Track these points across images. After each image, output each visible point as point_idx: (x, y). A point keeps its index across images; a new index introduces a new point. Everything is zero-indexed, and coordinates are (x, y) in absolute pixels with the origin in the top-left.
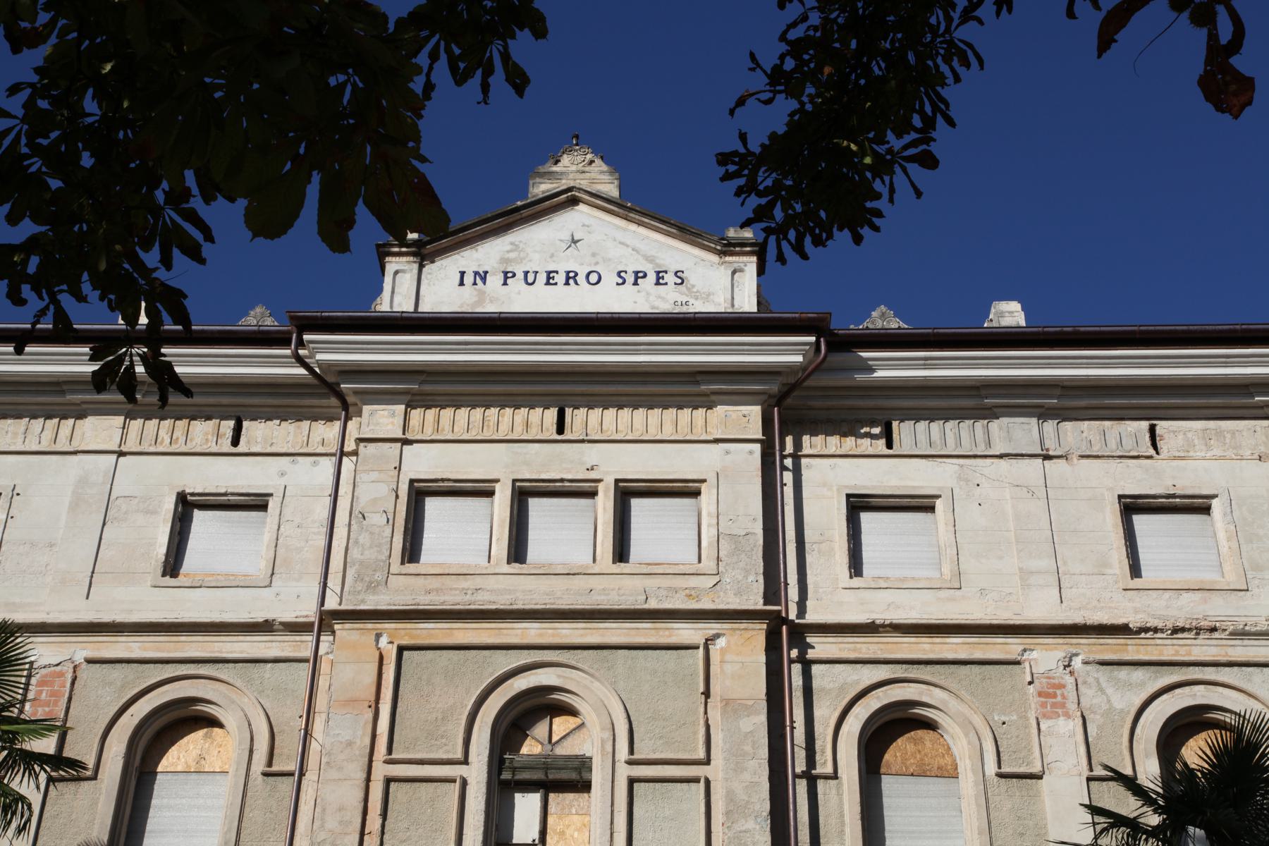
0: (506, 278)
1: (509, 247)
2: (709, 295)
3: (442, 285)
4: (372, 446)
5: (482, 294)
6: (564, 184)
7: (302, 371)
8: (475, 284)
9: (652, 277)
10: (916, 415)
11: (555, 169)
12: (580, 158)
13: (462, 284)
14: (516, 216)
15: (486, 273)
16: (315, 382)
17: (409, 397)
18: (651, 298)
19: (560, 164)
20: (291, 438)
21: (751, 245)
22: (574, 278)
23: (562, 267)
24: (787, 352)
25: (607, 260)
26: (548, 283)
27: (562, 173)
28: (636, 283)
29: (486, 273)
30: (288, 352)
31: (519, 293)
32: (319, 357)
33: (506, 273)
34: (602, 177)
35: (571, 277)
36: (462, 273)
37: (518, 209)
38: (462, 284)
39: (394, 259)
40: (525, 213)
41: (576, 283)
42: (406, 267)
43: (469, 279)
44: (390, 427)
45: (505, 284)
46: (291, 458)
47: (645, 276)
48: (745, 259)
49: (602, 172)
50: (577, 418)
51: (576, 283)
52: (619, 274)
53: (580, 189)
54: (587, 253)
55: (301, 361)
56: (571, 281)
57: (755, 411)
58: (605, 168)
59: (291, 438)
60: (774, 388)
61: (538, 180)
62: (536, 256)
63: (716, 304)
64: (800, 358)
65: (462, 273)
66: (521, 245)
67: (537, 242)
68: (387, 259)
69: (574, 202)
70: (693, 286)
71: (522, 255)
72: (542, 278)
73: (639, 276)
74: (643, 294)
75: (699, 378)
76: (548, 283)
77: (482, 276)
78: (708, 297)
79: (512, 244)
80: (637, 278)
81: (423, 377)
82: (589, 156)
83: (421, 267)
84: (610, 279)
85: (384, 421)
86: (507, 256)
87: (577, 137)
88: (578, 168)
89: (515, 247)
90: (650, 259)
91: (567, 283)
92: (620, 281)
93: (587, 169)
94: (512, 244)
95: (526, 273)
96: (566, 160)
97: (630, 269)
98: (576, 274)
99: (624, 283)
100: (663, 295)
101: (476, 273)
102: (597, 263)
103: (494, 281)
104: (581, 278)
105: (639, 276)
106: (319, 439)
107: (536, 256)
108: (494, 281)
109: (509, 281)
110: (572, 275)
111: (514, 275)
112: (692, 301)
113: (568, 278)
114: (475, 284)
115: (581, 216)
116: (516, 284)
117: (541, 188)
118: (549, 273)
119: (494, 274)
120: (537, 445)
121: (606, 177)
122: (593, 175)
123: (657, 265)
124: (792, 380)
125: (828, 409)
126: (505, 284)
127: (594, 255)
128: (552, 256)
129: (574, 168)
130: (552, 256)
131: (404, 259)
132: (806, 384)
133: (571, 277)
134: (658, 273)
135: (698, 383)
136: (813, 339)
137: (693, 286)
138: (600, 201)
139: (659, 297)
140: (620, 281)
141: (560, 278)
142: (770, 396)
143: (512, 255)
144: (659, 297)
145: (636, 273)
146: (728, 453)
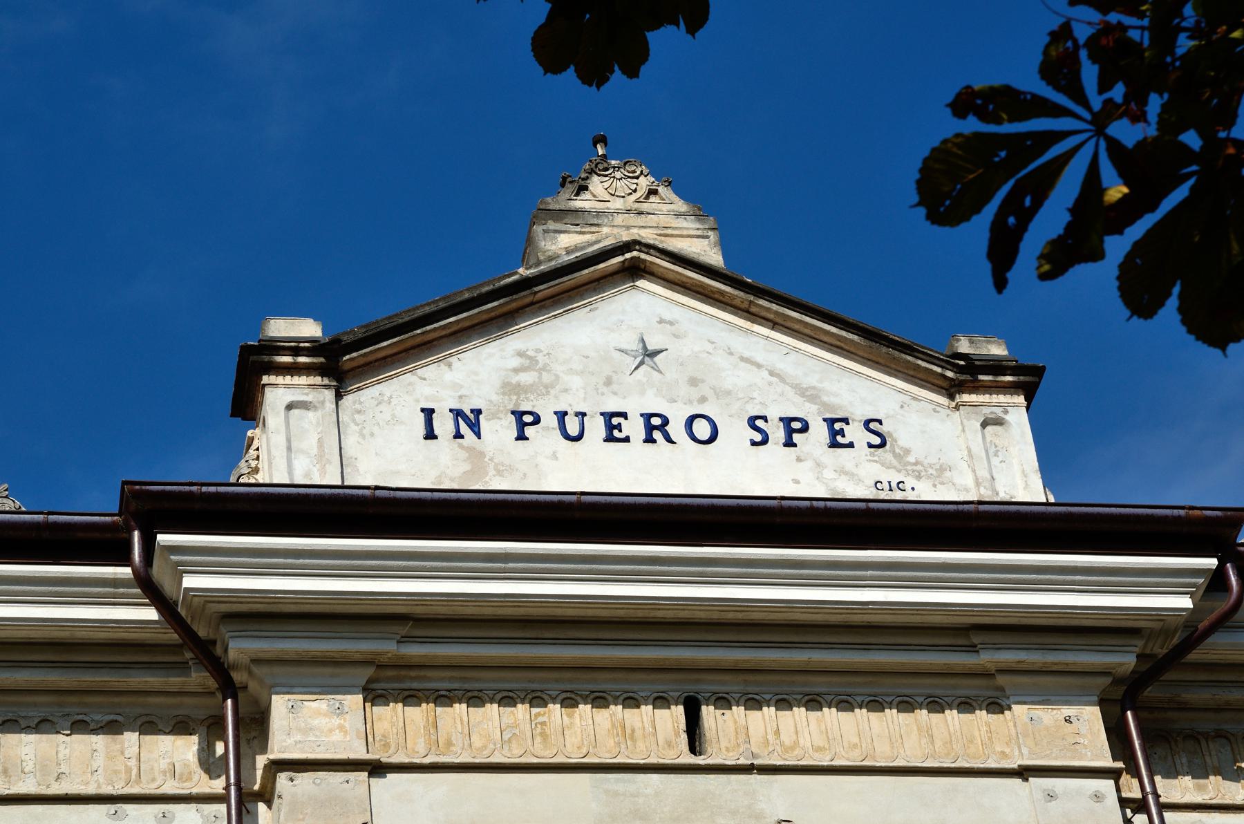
0: (522, 426)
1: (516, 362)
2: (942, 470)
3: (377, 436)
4: (305, 780)
5: (477, 457)
6: (609, 235)
7: (151, 614)
8: (458, 435)
9: (819, 431)
10: (320, 675)
11: (578, 204)
12: (622, 186)
13: (430, 435)
14: (524, 297)
15: (478, 412)
16: (173, 637)
17: (369, 672)
18: (828, 474)
19: (586, 195)
20: (99, 761)
21: (1015, 370)
22: (662, 427)
23: (635, 406)
24: (1158, 590)
25: (722, 394)
26: (610, 438)
27: (599, 213)
28: (789, 443)
29: (478, 412)
30: (125, 572)
31: (554, 456)
32: (189, 582)
33: (518, 414)
34: (681, 223)
35: (655, 427)
36: (429, 413)
37: (527, 283)
38: (430, 435)
39: (280, 380)
40: (543, 290)
41: (669, 440)
42: (310, 396)
43: (444, 425)
44: (337, 736)
45: (521, 437)
46: (111, 808)
47: (805, 429)
48: (1002, 399)
49: (678, 215)
50: (733, 729)
51: (669, 440)
52: (752, 422)
53: (649, 248)
54: (653, 382)
55: (151, 591)
56: (657, 435)
57: (1090, 718)
58: (681, 206)
59: (99, 761)
60: (1125, 660)
61: (552, 225)
62: (576, 382)
63: (957, 486)
64: (1186, 602)
65: (429, 413)
66: (541, 358)
67: (575, 348)
68: (265, 379)
69: (634, 271)
70: (907, 451)
71: (546, 378)
72: (596, 428)
73: (794, 428)
74: (809, 464)
75: (976, 639)
76: (610, 438)
77: (469, 420)
78: (940, 472)
79: (521, 354)
80: (790, 432)
81: (404, 630)
82: (644, 183)
83: (339, 396)
84: (735, 434)
85: (321, 722)
86: (515, 379)
87: (602, 140)
88: (621, 205)
89: (529, 362)
90: (809, 394)
91: (649, 440)
92: (758, 437)
93: (645, 207)
94: (521, 354)
95: (562, 416)
96: (597, 185)
97: (774, 413)
98: (666, 421)
99: (765, 441)
100: (849, 466)
101: (458, 414)
102: (703, 400)
103: (498, 430)
104: (676, 428)
105: (794, 428)
106: (164, 764)
107: (576, 382)
108: (498, 430)
109: (529, 431)
110: (656, 421)
111: (537, 421)
112: (910, 482)
113: (650, 429)
114: (458, 435)
115: (642, 308)
116: (544, 437)
117: (562, 243)
118: (608, 416)
119: (494, 416)
120: (655, 778)
121: (690, 225)
122: (664, 220)
123: (825, 406)
124: (1160, 650)
125: (1218, 709)
126: (521, 437)
127: (693, 382)
128: (608, 382)
129: (617, 204)
130: (608, 382)
131: (303, 380)
132: (1193, 656)
133: (655, 427)
134: (831, 422)
135: (973, 649)
136: (1212, 562)
137: (907, 451)
138: (688, 277)
139: (842, 472)
140: (758, 437)
141: (634, 428)
142: (1117, 681)
143: (526, 378)
144: (842, 472)
145: (787, 421)
146: (1051, 796)
